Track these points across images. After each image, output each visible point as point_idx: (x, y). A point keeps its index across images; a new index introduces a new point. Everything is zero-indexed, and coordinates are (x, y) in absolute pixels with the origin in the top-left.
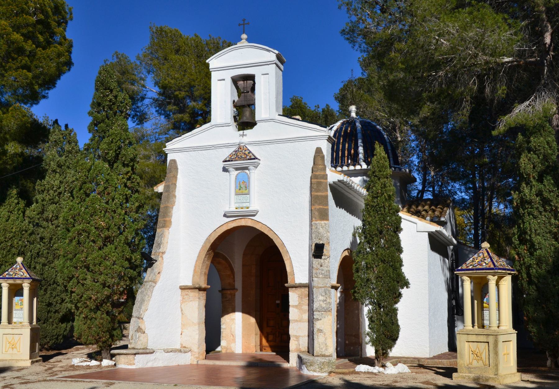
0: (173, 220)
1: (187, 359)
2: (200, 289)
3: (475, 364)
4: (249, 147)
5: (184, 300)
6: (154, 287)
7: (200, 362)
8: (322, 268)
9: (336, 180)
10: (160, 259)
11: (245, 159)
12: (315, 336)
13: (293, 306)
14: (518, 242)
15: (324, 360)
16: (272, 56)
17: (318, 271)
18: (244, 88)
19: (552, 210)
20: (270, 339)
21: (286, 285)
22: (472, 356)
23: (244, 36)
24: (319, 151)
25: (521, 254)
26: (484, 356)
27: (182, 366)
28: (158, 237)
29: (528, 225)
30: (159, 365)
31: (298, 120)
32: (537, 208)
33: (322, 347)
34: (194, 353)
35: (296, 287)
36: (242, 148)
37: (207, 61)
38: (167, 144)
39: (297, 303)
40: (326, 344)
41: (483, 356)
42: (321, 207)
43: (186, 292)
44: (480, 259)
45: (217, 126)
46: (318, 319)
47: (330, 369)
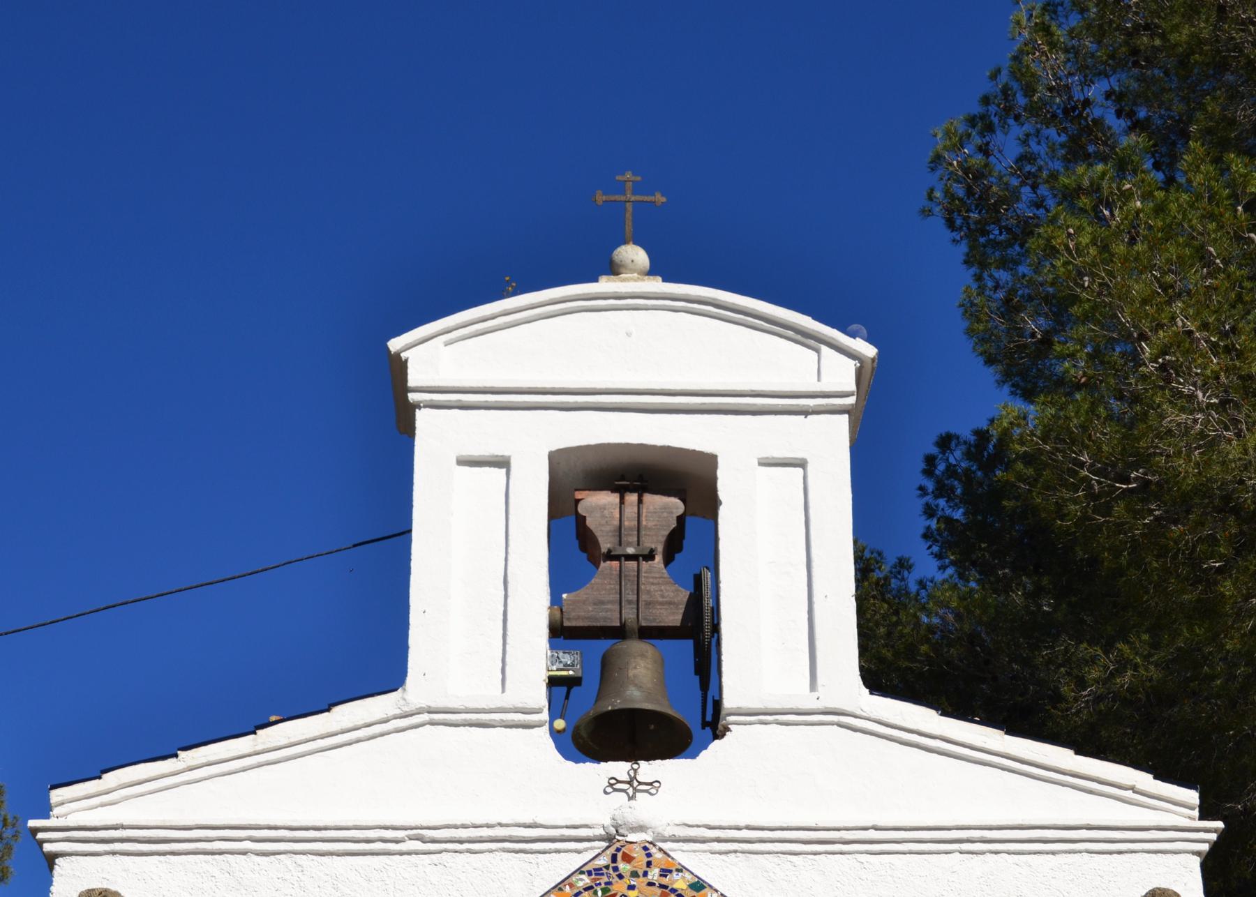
4: (682, 855)
36: (638, 854)
37: (395, 344)
38: (56, 795)
45: (441, 716)
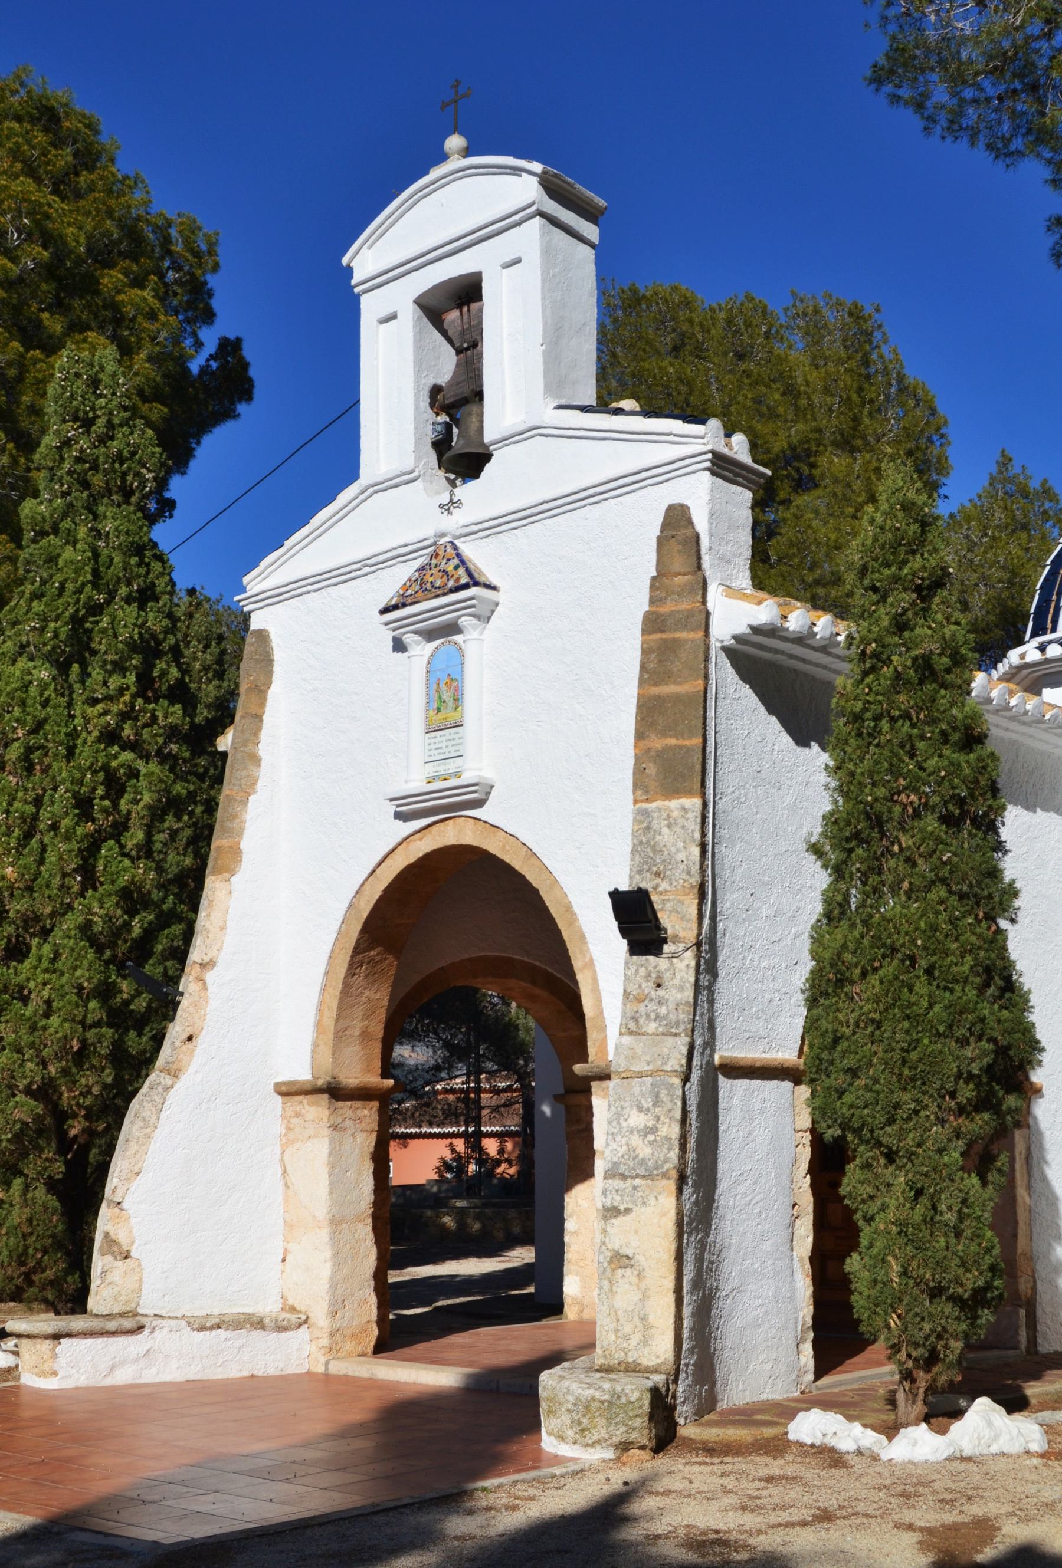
0: (246, 844)
1: (297, 1354)
2: (335, 1092)
5: (291, 1135)
6: (167, 1089)
7: (338, 1368)
8: (661, 992)
9: (742, 628)
15: (590, 1392)
16: (519, 186)
17: (642, 1008)
18: (463, 332)
21: (578, 1068)
23: (455, 142)
24: (677, 519)
27: (266, 1379)
30: (166, 1377)
31: (632, 413)
33: (627, 1329)
34: (317, 1333)
40: (644, 1319)
42: (673, 742)
47: (619, 1434)
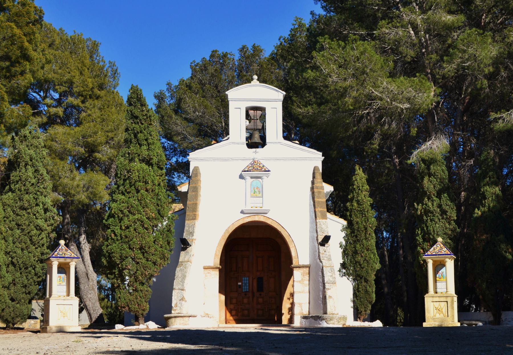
3: (438, 316)
4: (262, 161)
10: (193, 244)
11: (261, 170)
12: (328, 301)
13: (297, 282)
14: (422, 240)
19: (447, 218)
20: (233, 314)
22: (435, 311)
25: (425, 249)
26: (444, 310)
28: (189, 227)
29: (431, 228)
32: (437, 216)
35: (299, 267)
37: (226, 93)
39: (300, 279)
41: (444, 311)
43: (208, 271)
44: (438, 248)
45: (234, 143)
46: (328, 289)
